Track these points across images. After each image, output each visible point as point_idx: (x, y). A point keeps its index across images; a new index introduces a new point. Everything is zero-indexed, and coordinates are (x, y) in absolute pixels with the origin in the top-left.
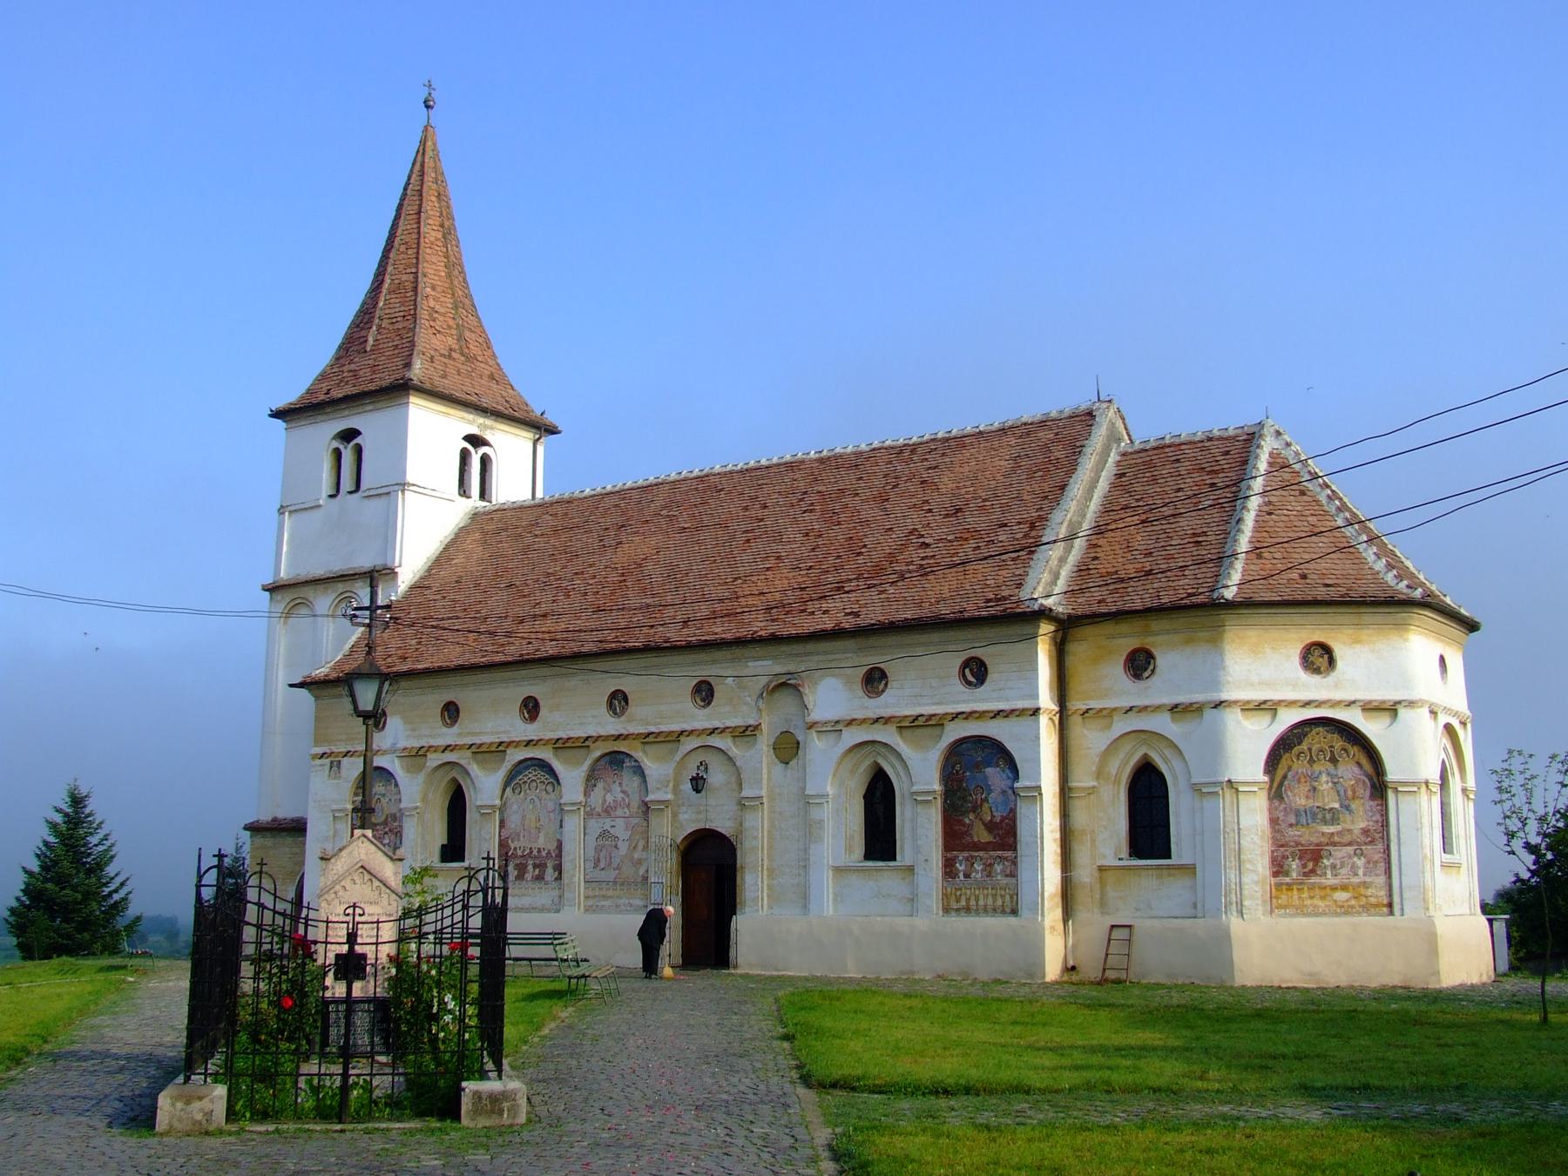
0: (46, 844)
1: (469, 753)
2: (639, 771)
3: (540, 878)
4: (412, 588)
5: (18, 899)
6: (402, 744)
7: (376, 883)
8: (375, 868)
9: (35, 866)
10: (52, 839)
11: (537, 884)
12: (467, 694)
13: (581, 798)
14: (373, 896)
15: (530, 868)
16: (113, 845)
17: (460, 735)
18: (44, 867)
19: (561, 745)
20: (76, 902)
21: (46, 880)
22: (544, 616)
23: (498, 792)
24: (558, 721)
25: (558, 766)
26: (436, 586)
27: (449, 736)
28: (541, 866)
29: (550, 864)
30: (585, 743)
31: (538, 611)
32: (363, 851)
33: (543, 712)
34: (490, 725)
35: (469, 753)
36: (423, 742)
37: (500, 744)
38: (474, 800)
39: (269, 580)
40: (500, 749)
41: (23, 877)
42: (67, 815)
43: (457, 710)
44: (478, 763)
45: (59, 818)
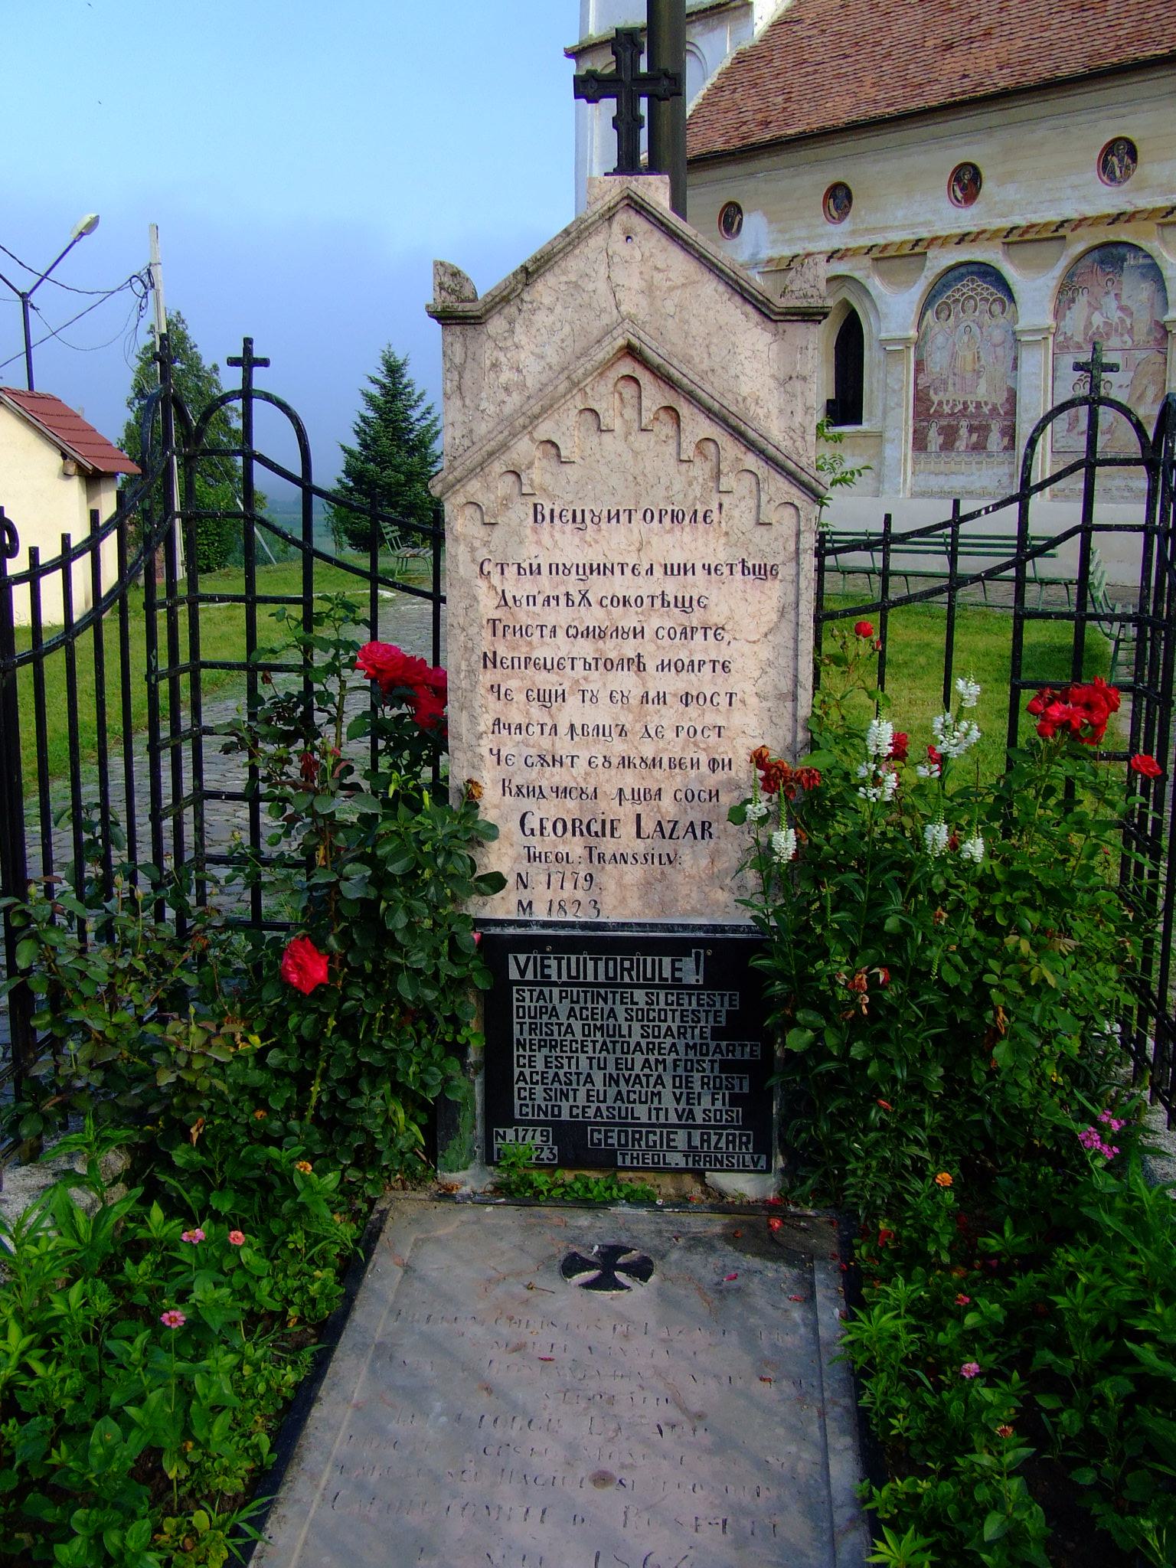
0: (364, 419)
1: (867, 261)
2: (1154, 273)
3: (979, 447)
4: (774, 26)
5: (339, 481)
6: (766, 253)
7: (697, 426)
8: (691, 359)
9: (354, 444)
10: (370, 414)
11: (975, 457)
12: (864, 168)
13: (1049, 321)
14: (683, 485)
15: (963, 432)
16: (436, 419)
17: (853, 233)
18: (365, 446)
19: (1016, 238)
20: (399, 484)
21: (367, 460)
22: (987, 34)
23: (913, 318)
24: (1007, 202)
25: (1011, 272)
26: (810, 17)
27: (837, 235)
28: (982, 430)
29: (995, 427)
30: (1057, 233)
31: (976, 28)
32: (631, 280)
33: (988, 187)
34: (900, 214)
35: (867, 261)
36: (797, 249)
37: (918, 242)
38: (874, 332)
39: (573, 42)
40: (916, 251)
41: (342, 457)
42: (383, 386)
43: (849, 196)
44: (882, 275)
45: (375, 391)
